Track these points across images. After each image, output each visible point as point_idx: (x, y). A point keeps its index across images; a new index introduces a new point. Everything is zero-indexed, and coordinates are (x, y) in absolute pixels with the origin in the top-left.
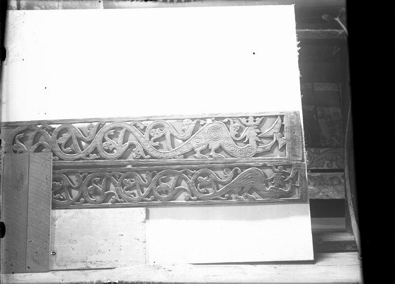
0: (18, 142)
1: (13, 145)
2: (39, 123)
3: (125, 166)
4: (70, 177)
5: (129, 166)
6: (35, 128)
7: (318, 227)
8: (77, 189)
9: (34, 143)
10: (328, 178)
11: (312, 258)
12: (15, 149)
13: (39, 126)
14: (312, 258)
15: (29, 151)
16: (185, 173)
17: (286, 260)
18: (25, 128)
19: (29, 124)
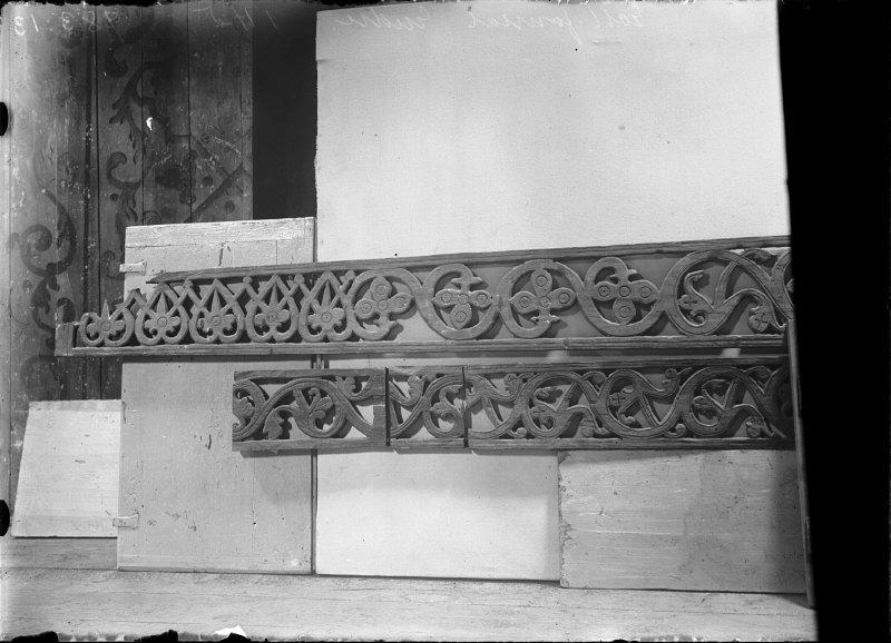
0: (690, 288)
1: (679, 297)
2: (739, 243)
3: (719, 350)
4: (492, 381)
5: (732, 353)
6: (731, 257)
7: (246, 198)
8: (409, 408)
9: (729, 293)
10: (330, 327)
11: (127, 367)
12: (686, 306)
13: (739, 251)
14: (127, 367)
15: (719, 310)
16: (753, 375)
17: (136, 365)
18: (705, 256)
19: (713, 247)
